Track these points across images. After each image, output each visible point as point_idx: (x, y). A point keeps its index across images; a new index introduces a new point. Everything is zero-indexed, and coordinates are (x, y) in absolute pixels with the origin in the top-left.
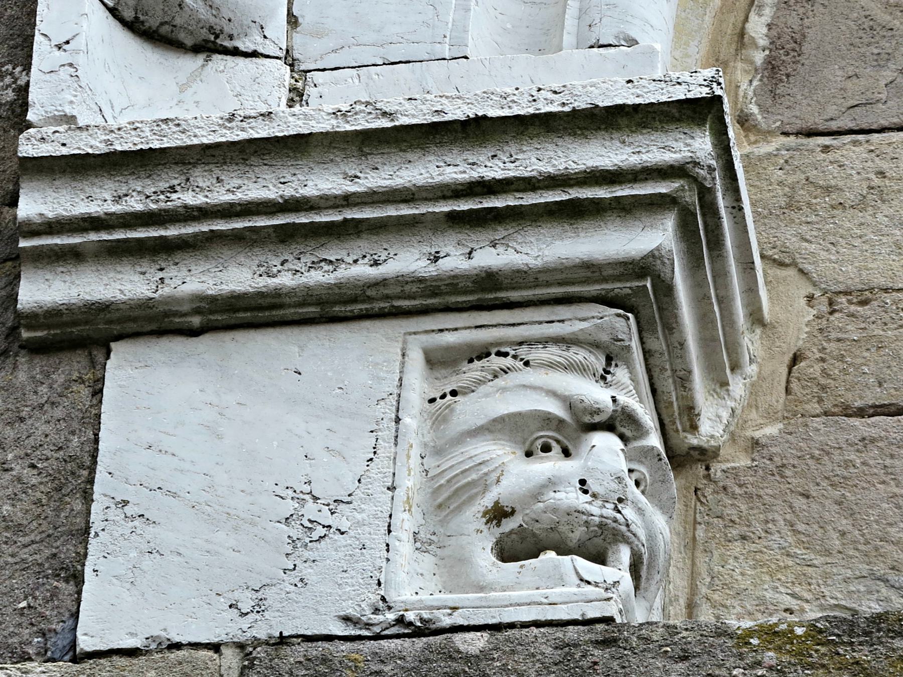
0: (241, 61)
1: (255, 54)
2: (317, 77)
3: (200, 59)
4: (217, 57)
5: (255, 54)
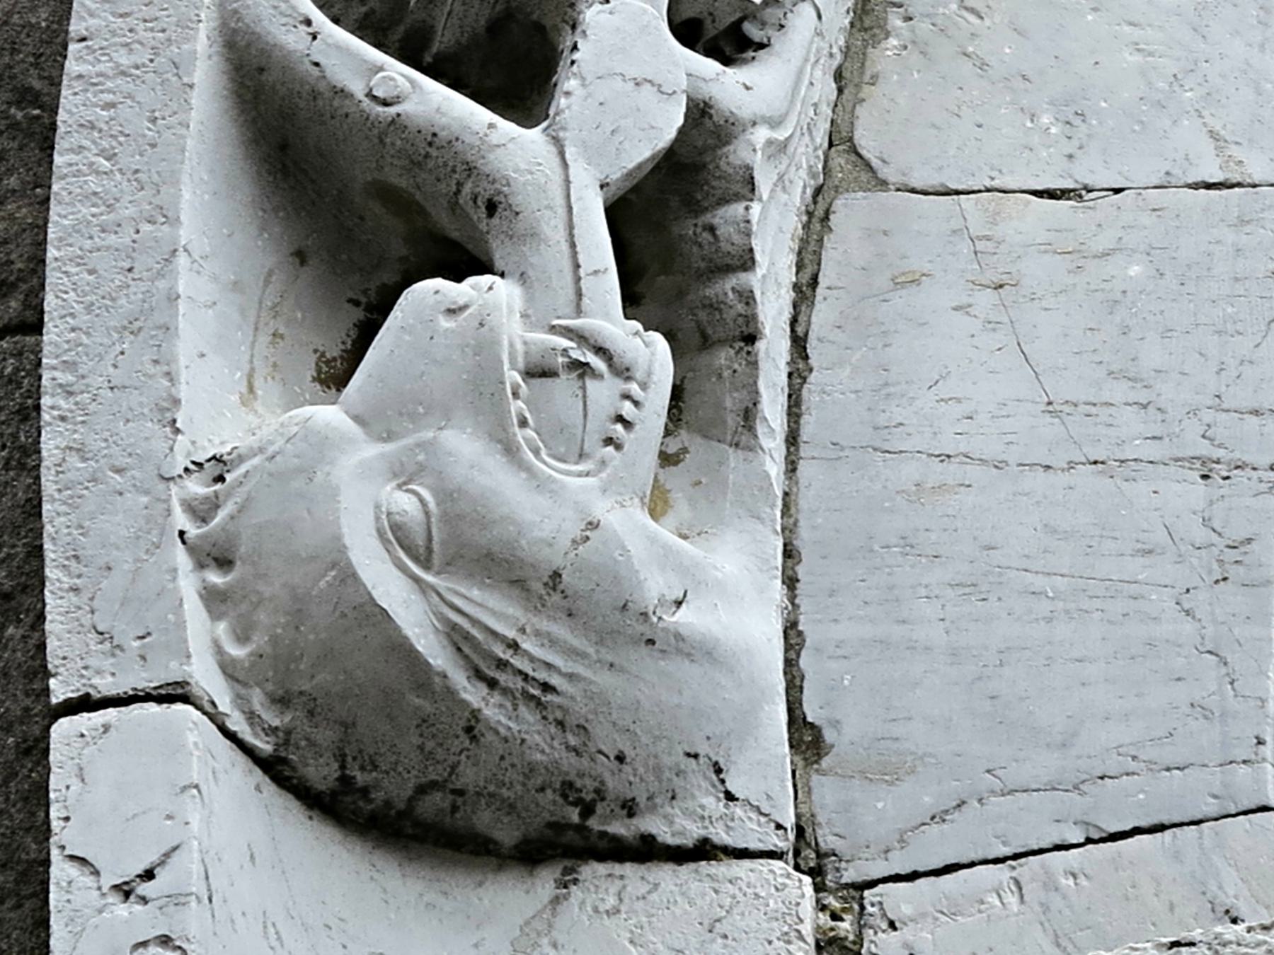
0: (666, 875)
1: (704, 851)
2: (897, 898)
3: (545, 882)
4: (593, 871)
5: (704, 851)
